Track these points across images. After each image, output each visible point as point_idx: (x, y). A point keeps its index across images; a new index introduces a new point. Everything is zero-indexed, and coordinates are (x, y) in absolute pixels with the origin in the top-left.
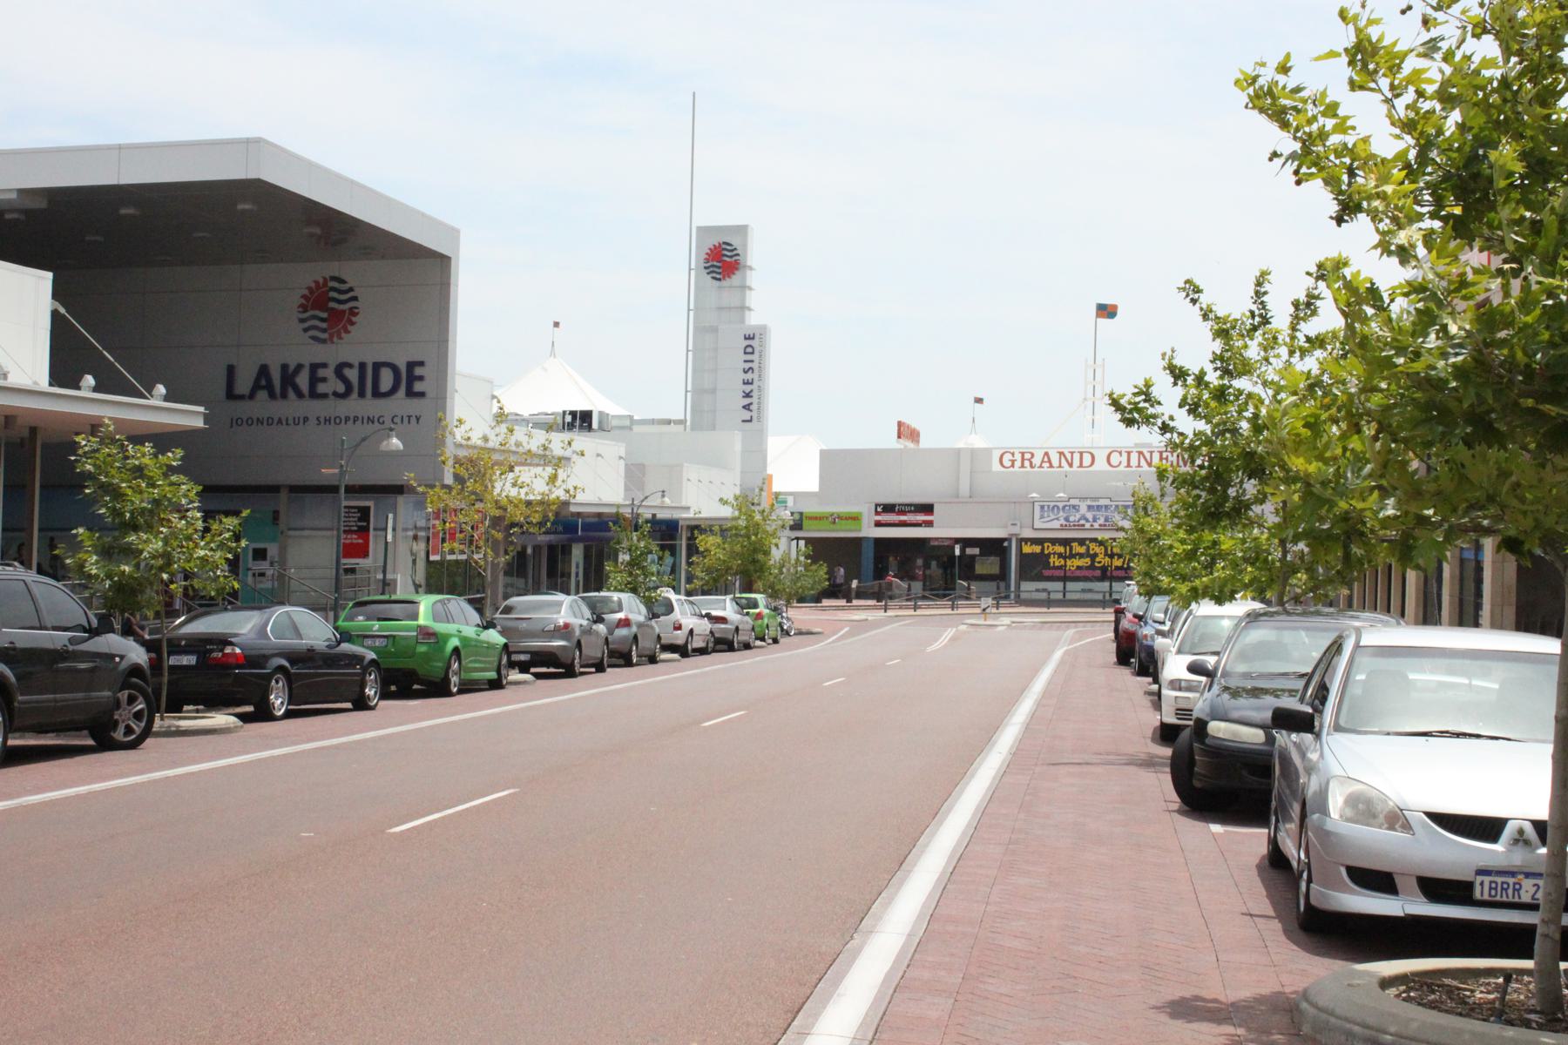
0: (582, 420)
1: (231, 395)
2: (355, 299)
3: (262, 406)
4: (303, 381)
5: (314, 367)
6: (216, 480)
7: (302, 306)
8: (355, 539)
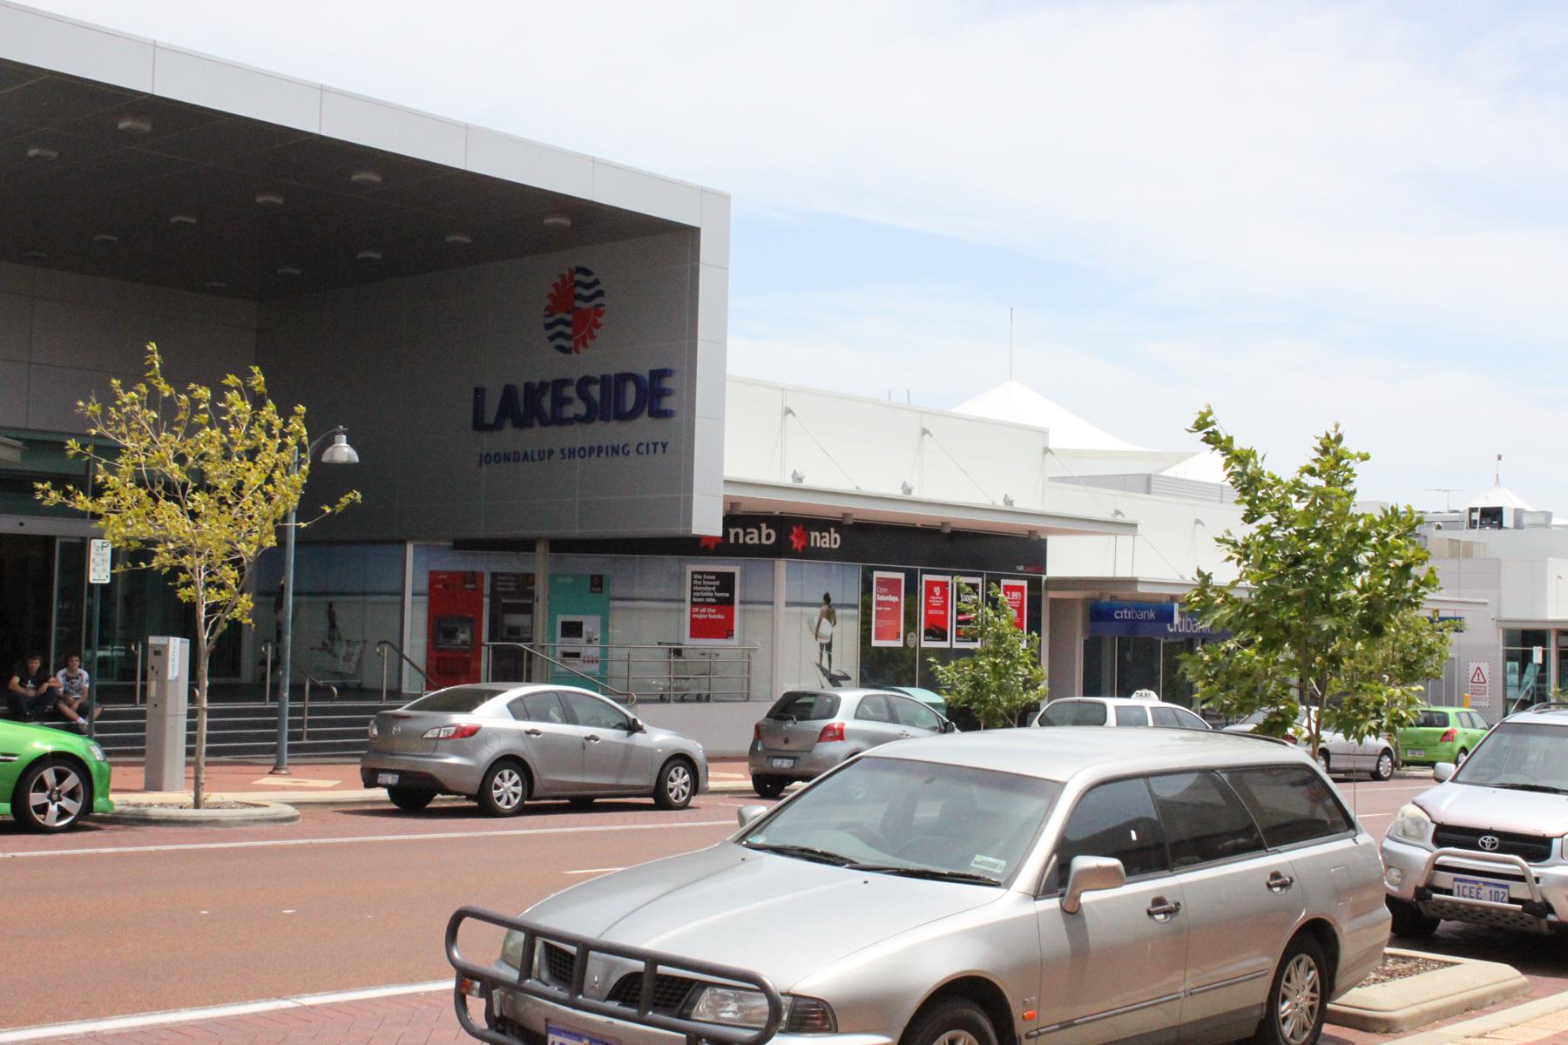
0: (1492, 516)
1: (479, 425)
2: (600, 293)
3: (510, 438)
4: (547, 403)
5: (561, 384)
6: (468, 533)
7: (600, 314)
8: (714, 615)
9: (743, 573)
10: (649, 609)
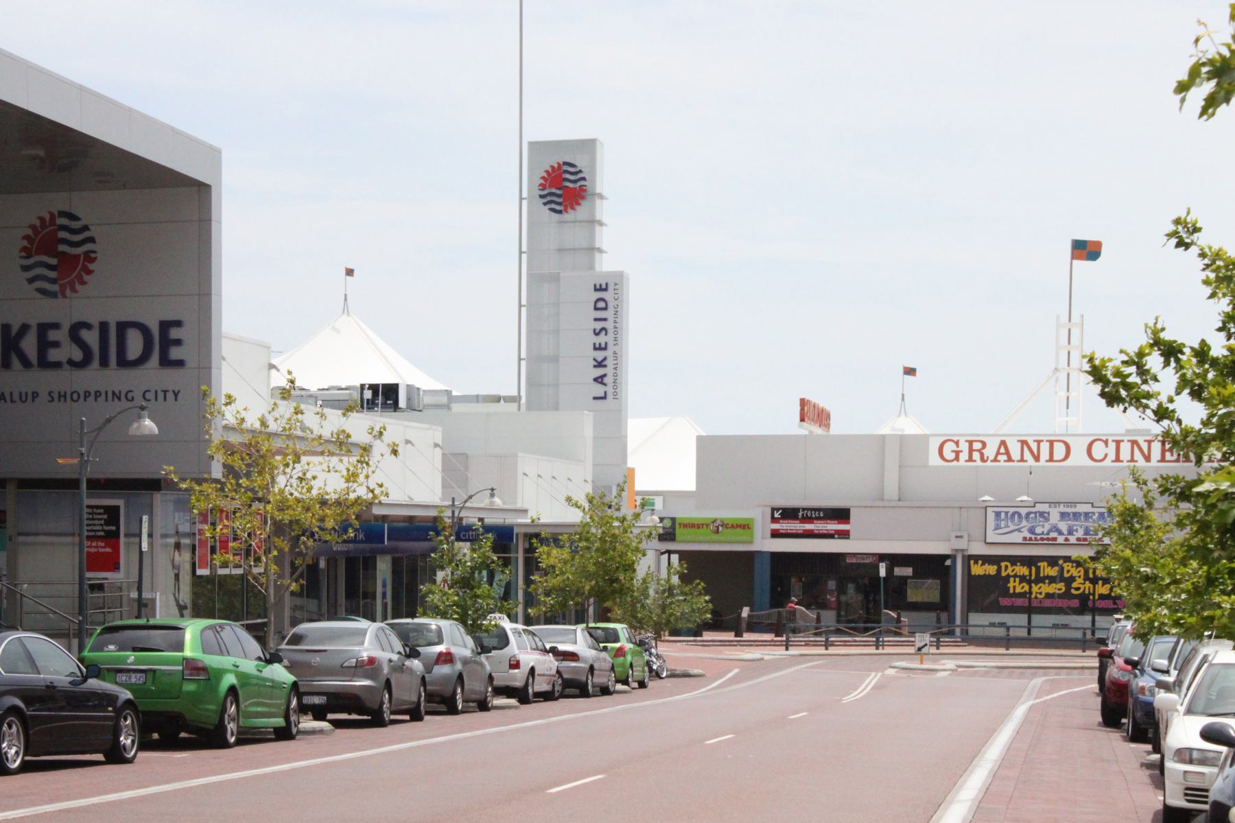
0: (385, 396)
5: (43, 328)
8: (103, 548)
9: (127, 506)
10: (45, 544)
